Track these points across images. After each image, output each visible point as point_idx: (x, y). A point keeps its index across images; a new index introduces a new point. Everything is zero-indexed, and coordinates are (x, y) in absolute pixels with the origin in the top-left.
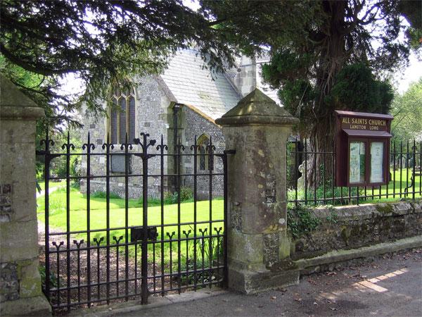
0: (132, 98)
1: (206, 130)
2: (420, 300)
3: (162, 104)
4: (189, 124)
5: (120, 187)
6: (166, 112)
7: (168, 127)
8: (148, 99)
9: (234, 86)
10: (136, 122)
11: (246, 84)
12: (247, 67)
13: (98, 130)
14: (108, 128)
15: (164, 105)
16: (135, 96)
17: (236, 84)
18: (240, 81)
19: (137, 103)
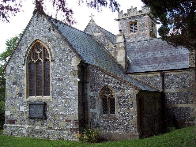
0: (47, 60)
1: (108, 82)
2: (1, 77)
3: (72, 63)
4: (93, 79)
5: (37, 130)
6: (76, 69)
7: (78, 80)
8: (61, 60)
9: (112, 57)
10: (51, 78)
11: (121, 55)
12: (120, 44)
13: (19, 86)
14: (27, 83)
15: (75, 62)
16: (50, 59)
17: (113, 55)
18: (116, 53)
19: (51, 64)
